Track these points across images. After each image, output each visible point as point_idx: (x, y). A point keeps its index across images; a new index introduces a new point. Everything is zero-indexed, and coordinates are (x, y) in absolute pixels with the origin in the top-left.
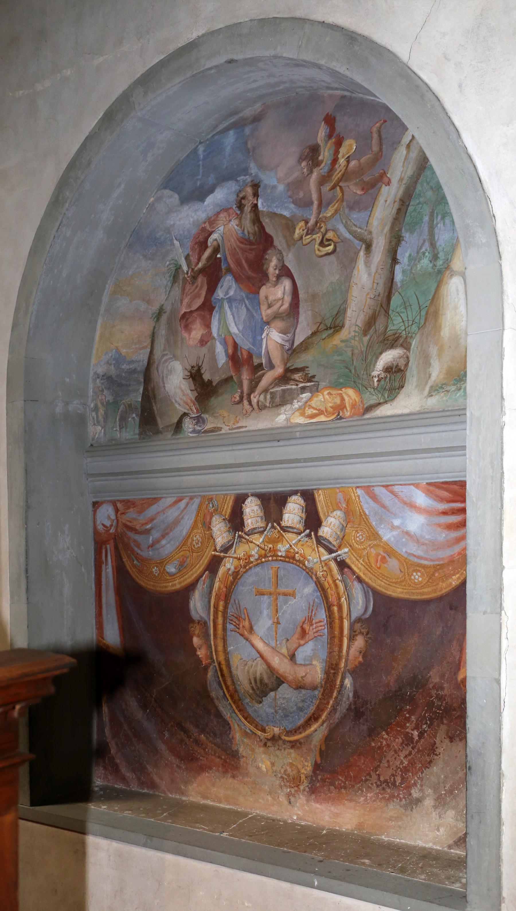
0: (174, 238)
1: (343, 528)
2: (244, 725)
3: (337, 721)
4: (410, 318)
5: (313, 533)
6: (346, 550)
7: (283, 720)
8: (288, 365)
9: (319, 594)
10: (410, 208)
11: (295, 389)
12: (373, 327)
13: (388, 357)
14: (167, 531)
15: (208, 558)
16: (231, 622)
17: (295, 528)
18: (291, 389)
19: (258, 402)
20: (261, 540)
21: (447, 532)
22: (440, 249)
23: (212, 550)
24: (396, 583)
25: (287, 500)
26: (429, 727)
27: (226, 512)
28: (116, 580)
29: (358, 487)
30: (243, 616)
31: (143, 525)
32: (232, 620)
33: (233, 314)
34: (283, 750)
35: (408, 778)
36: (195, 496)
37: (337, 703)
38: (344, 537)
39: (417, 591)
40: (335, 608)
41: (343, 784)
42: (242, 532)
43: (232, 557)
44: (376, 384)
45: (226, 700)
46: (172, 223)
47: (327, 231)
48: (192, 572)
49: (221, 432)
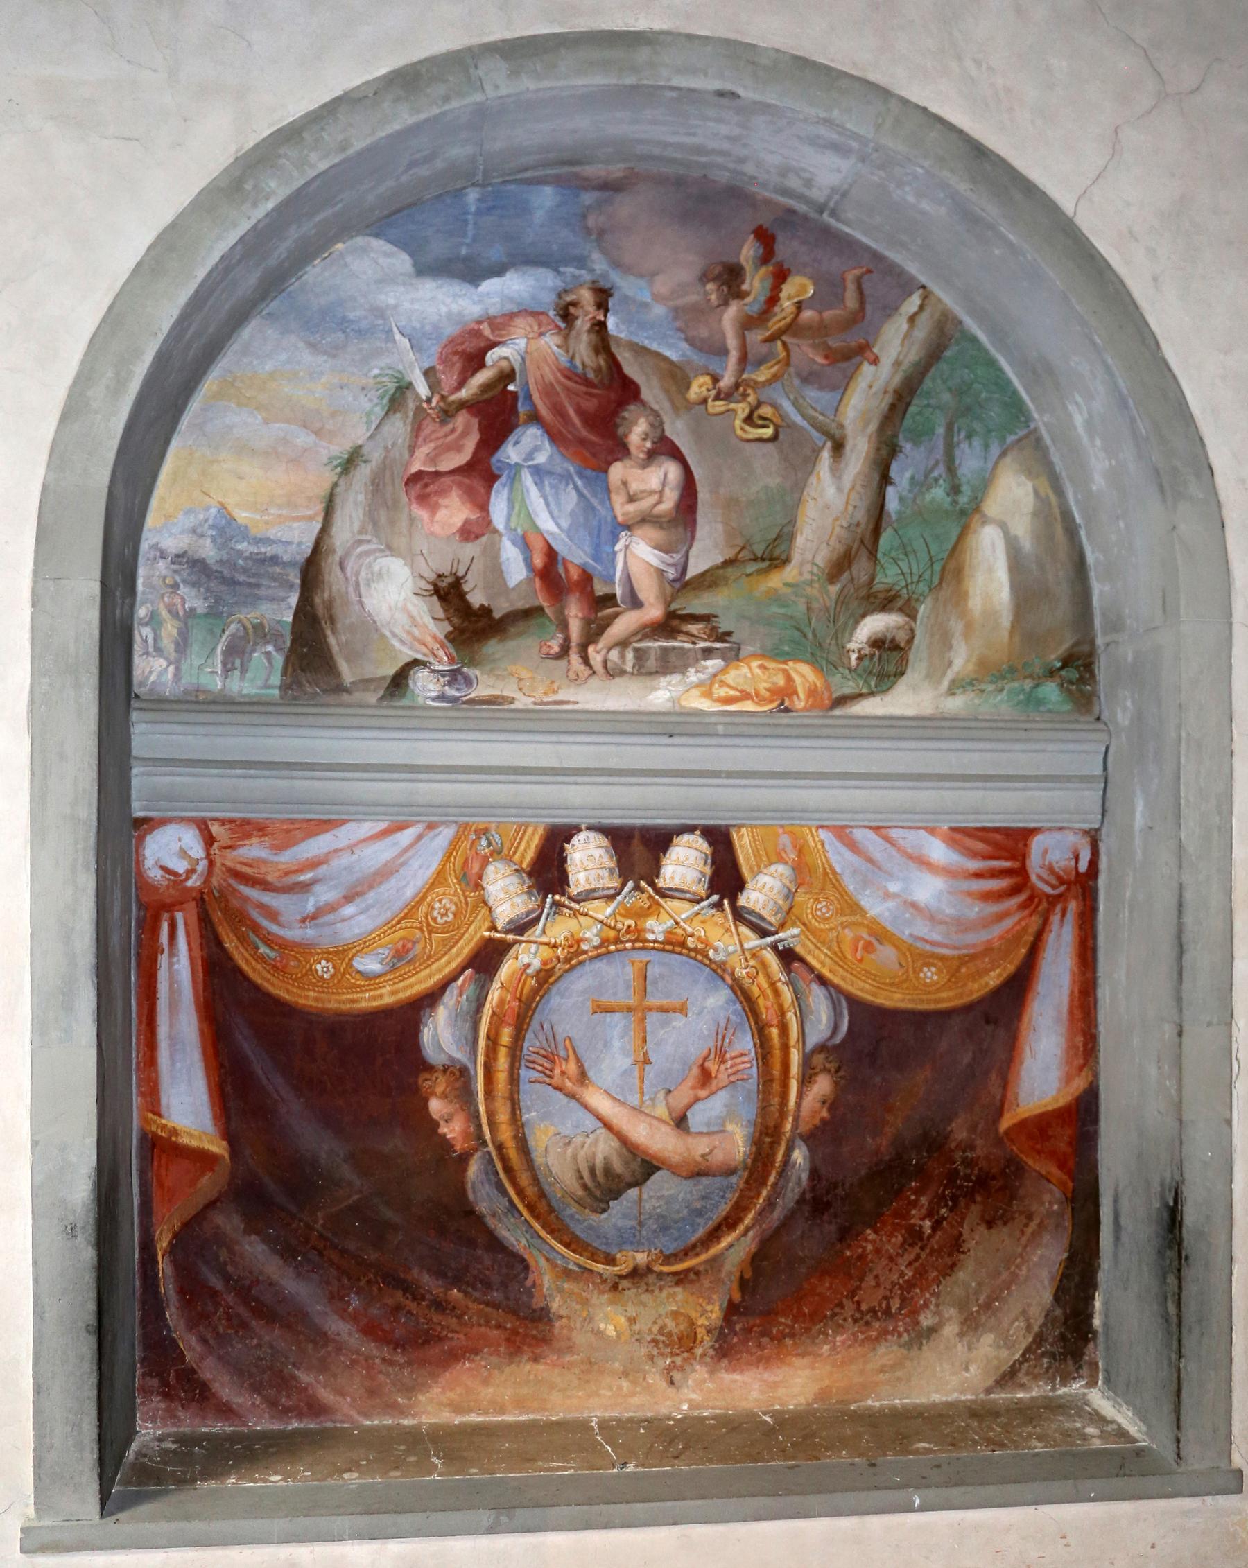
0: (395, 329)
1: (789, 895)
2: (564, 1257)
3: (777, 1223)
4: (915, 570)
5: (726, 902)
6: (796, 931)
7: (657, 1237)
8: (674, 606)
9: (739, 1007)
10: (912, 409)
11: (689, 650)
12: (846, 574)
13: (875, 624)
14: (358, 889)
15: (472, 944)
16: (531, 1065)
17: (688, 892)
18: (682, 648)
19: (605, 662)
20: (609, 911)
21: (982, 905)
22: (964, 480)
23: (483, 928)
24: (891, 985)
25: (671, 840)
26: (951, 1210)
27: (523, 856)
28: (200, 987)
29: (822, 827)
30: (562, 1053)
31: (287, 873)
32: (533, 1062)
33: (545, 498)
34: (657, 1292)
35: (912, 1298)
36: (443, 823)
37: (777, 1191)
38: (791, 908)
39: (930, 997)
40: (774, 1032)
41: (787, 1330)
42: (563, 894)
43: (535, 942)
44: (854, 663)
45: (517, 1215)
46: (392, 301)
47: (759, 404)
48: (428, 971)
49: (512, 706)
